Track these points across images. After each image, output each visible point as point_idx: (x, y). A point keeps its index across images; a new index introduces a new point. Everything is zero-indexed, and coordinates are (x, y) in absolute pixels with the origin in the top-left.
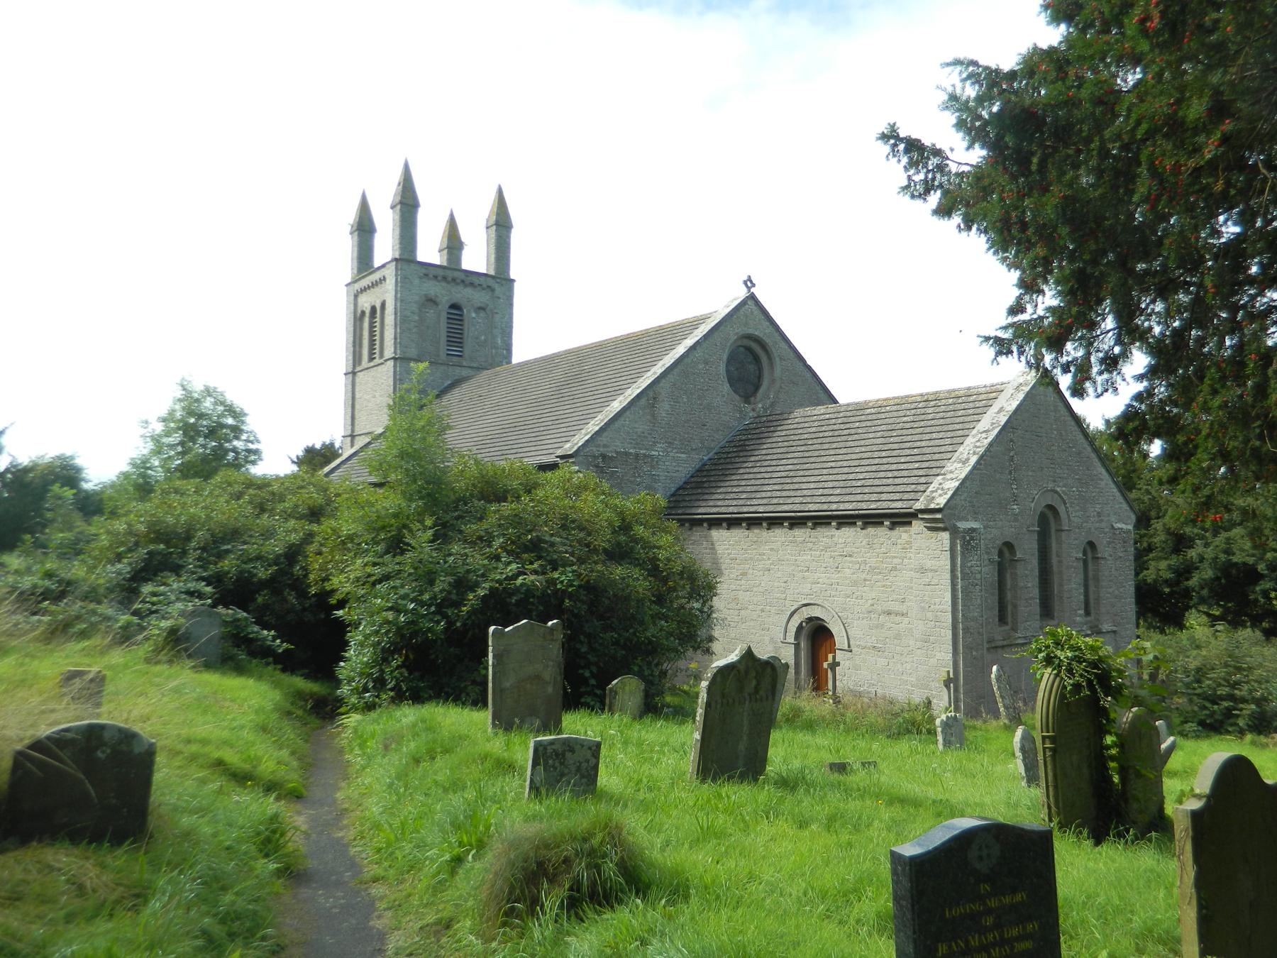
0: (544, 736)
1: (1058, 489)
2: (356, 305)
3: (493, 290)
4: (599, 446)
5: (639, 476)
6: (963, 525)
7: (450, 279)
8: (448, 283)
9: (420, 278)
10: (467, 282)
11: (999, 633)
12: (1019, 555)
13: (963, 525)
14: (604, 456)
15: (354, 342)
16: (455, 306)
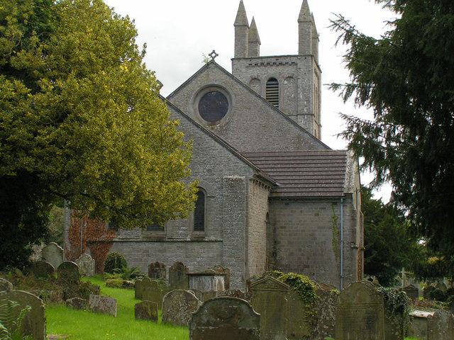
8: (265, 66)
16: (272, 79)
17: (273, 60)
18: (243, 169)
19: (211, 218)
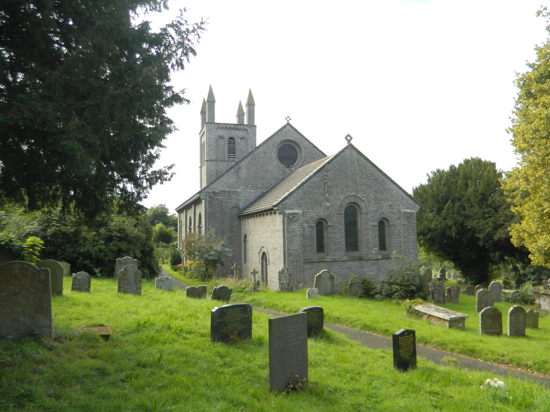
0: (49, 285)
1: (359, 195)
2: (201, 141)
3: (247, 130)
4: (212, 188)
5: (231, 199)
6: (287, 212)
7: (228, 128)
8: (228, 129)
9: (216, 129)
10: (243, 129)
11: (316, 257)
12: (329, 224)
13: (287, 212)
14: (214, 193)
15: (201, 155)
16: (231, 138)
17: (224, 126)
18: (412, 205)
19: (391, 240)
